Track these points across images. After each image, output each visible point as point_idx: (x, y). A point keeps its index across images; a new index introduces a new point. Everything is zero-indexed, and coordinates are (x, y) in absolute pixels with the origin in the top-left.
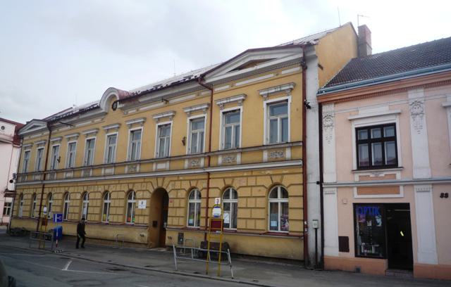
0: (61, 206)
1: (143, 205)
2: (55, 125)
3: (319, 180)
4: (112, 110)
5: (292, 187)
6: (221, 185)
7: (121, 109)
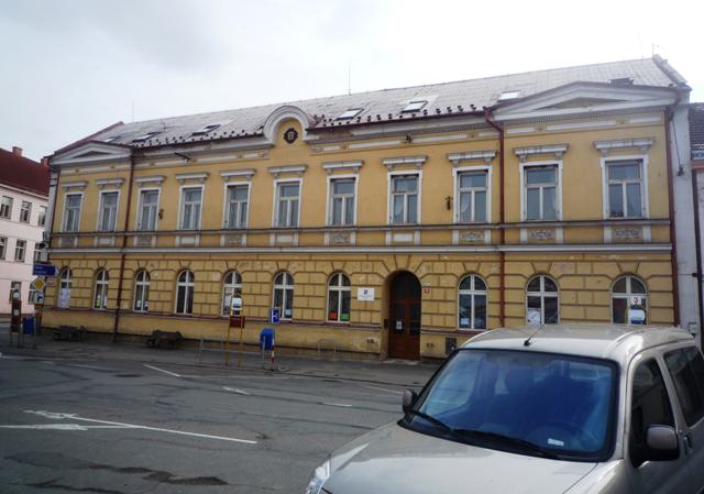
0: (173, 292)
1: (367, 295)
2: (146, 154)
3: (695, 271)
4: (285, 143)
5: (564, 278)
6: (135, 268)
7: (308, 142)
